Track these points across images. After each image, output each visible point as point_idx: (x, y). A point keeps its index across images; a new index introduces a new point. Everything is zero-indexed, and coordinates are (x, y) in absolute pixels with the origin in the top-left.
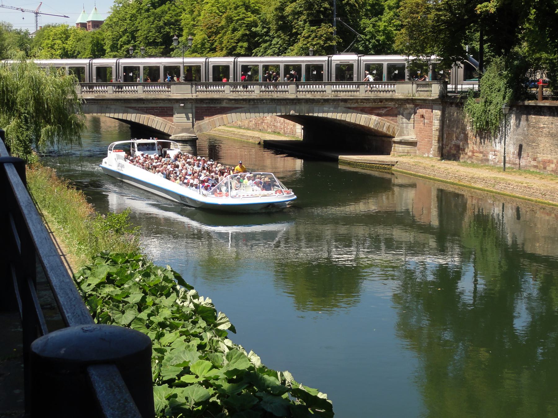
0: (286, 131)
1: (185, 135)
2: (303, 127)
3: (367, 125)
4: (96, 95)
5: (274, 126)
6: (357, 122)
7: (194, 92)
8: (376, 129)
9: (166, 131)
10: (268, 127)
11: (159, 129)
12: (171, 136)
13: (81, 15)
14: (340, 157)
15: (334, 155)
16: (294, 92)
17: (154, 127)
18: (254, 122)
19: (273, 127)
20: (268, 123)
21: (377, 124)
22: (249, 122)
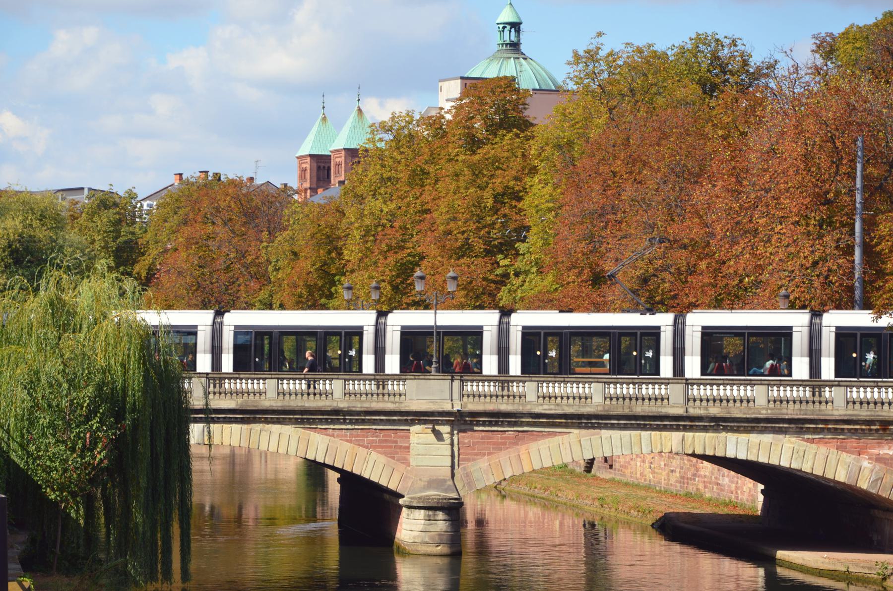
0: (740, 497)
1: (434, 494)
2: (761, 487)
3: (853, 483)
4: (240, 400)
5: (718, 484)
6: (829, 475)
7: (456, 395)
8: (874, 491)
9: (392, 486)
10: (705, 487)
11: (376, 481)
12: (402, 496)
13: (315, 129)
14: (781, 554)
15: (767, 550)
16: (682, 400)
17: (366, 475)
18: (678, 475)
19: (715, 487)
20: (705, 476)
21: (877, 480)
22: (668, 475)
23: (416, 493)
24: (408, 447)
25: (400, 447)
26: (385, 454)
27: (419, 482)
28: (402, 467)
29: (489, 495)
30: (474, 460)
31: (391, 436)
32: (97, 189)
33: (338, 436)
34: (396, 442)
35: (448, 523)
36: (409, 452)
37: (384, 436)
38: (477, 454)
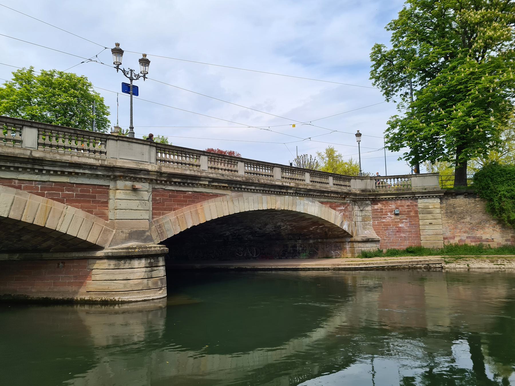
23: (118, 244)
24: (107, 202)
25: (98, 202)
26: (82, 208)
27: (121, 234)
28: (101, 222)
29: (152, 266)
30: (163, 214)
31: (89, 192)
32: (173, 141)
33: (26, 188)
34: (94, 197)
35: (86, 306)
36: (107, 206)
37: (81, 191)
38: (165, 210)
